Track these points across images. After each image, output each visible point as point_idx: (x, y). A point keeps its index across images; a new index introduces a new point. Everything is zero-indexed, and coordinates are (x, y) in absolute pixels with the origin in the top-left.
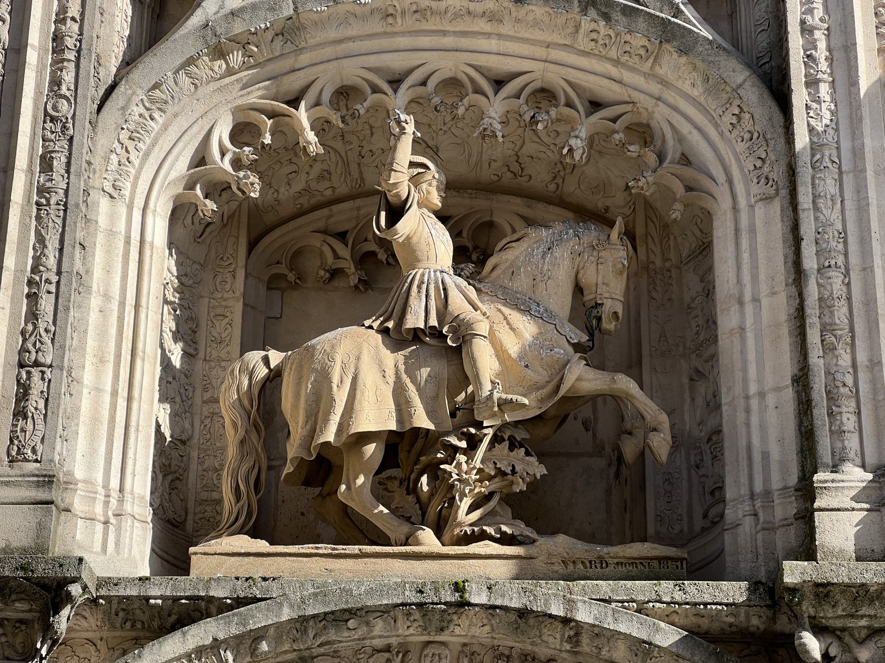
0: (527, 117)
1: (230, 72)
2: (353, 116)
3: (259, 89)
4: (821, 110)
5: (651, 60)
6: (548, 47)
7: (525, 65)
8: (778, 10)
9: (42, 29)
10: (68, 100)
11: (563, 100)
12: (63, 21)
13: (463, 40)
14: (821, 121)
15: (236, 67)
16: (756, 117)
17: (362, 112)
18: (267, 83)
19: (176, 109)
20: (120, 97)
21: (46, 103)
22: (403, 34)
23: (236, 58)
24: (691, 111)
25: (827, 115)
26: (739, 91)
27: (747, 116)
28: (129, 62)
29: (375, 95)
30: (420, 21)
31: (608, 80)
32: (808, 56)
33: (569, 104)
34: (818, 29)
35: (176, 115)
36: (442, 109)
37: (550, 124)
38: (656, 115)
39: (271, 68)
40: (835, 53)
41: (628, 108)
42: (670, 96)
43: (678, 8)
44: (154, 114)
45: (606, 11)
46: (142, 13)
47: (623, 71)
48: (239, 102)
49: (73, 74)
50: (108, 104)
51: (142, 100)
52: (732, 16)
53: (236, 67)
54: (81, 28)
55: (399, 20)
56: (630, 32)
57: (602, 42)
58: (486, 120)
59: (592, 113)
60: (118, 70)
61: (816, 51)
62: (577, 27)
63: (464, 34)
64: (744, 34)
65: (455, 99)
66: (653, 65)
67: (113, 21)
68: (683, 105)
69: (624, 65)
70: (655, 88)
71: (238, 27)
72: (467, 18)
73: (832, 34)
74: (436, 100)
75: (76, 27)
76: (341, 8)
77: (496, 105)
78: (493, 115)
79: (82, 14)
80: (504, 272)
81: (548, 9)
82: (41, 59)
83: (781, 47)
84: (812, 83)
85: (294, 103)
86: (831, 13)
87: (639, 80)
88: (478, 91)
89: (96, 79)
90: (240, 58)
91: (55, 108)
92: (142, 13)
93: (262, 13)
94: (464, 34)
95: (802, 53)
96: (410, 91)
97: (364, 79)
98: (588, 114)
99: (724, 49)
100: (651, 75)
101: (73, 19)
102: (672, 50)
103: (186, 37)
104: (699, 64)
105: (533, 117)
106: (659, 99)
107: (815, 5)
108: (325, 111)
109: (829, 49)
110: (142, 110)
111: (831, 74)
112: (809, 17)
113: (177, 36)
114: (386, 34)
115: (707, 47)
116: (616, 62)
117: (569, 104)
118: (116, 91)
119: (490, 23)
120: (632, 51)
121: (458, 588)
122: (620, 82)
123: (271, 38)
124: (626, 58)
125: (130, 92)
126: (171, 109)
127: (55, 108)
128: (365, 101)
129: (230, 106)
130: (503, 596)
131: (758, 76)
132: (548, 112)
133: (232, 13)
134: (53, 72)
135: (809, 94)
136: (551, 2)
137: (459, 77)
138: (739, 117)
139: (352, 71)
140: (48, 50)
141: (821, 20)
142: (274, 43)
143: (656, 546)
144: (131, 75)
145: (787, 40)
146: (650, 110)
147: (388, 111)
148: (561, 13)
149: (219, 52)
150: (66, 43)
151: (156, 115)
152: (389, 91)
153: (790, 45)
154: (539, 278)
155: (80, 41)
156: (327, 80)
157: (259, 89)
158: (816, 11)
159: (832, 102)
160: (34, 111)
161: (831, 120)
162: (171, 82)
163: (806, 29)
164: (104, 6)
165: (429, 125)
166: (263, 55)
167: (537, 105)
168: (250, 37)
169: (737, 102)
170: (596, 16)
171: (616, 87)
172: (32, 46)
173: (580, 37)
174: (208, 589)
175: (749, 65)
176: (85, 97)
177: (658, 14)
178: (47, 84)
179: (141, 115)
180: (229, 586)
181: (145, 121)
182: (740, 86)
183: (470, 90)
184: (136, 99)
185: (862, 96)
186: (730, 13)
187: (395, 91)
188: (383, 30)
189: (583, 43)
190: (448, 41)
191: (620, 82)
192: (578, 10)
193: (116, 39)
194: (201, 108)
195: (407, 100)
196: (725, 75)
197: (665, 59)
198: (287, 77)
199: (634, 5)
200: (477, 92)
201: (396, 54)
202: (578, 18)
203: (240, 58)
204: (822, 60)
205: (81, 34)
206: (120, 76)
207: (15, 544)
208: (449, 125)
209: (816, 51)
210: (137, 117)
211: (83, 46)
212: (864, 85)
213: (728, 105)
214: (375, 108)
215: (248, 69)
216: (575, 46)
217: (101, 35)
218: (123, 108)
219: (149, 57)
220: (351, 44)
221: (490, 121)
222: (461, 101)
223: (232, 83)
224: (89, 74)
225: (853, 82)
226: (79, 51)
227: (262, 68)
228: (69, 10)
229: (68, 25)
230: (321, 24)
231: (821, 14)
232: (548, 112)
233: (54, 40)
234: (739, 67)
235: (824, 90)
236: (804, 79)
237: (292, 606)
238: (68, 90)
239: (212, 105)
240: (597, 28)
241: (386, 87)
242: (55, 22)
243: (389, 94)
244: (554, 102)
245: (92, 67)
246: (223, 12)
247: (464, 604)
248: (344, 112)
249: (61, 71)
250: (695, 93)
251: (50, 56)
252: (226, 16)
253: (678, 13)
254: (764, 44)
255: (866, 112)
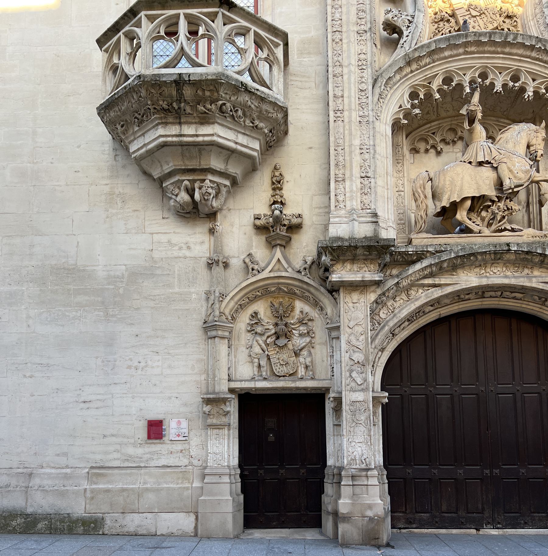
80: (503, 142)
121: (508, 245)
130: (522, 247)
143: (354, 279)
154: (516, 143)
174: (427, 248)
180: (434, 247)
207: (368, 236)
237: (454, 253)
247: (509, 250)
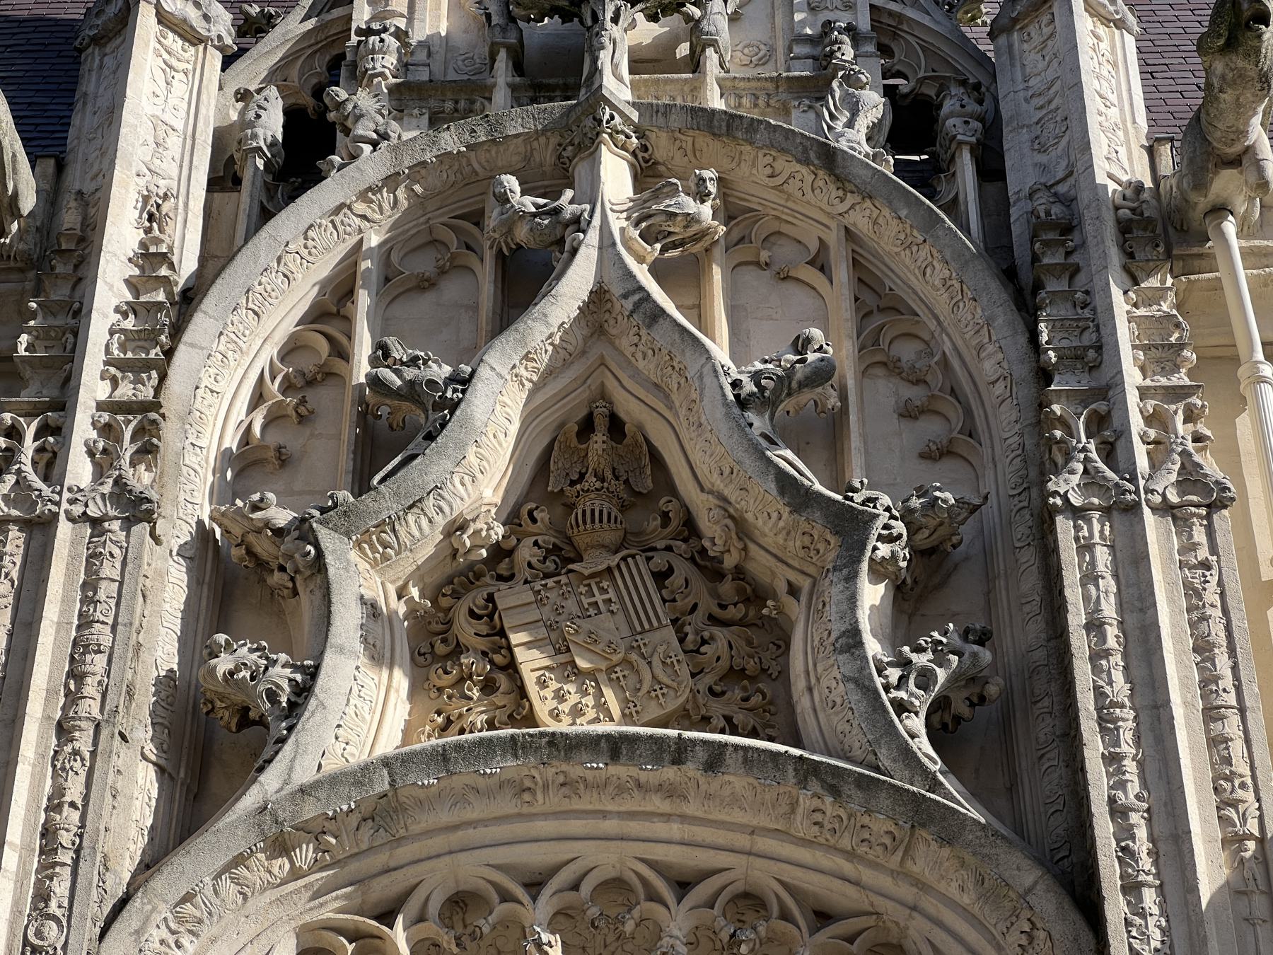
0: (725, 936)
1: (296, 874)
2: (473, 936)
3: (337, 898)
4: (1147, 928)
5: (900, 853)
6: (752, 833)
7: (722, 859)
8: (1076, 783)
9: (26, 819)
10: (58, 922)
11: (775, 910)
12: (58, 808)
13: (632, 824)
14: (1149, 944)
15: (305, 867)
16: (1056, 936)
17: (486, 929)
18: (349, 889)
19: (215, 930)
20: (134, 917)
21: (27, 927)
22: (545, 816)
23: (305, 854)
24: (962, 927)
25: (1157, 935)
26: (1028, 899)
27: (1041, 935)
28: (149, 865)
29: (505, 905)
30: (569, 797)
31: (840, 882)
32: (1124, 849)
33: (785, 916)
34: (1134, 810)
35: (213, 941)
36: (602, 924)
37: (758, 946)
38: (912, 932)
39: (354, 867)
40: (1160, 845)
41: (871, 921)
42: (929, 904)
43: (935, 779)
44: (181, 940)
45: (833, 782)
46: (173, 794)
47: (860, 868)
48: (307, 918)
49: (68, 884)
50: (116, 926)
51: (165, 919)
52: (1012, 789)
53: (305, 867)
54: (83, 818)
55: (540, 796)
56: (869, 812)
57: (830, 826)
58: (666, 941)
59: (819, 929)
60: (133, 876)
61: (1134, 842)
62: (794, 806)
63: (632, 815)
64: (1030, 816)
65: (620, 910)
66: (903, 859)
67: (130, 806)
68: (949, 917)
69: (862, 859)
70: (906, 891)
71: (310, 811)
72: (636, 793)
73: (1155, 817)
74: (594, 911)
75: (75, 816)
76: (457, 781)
77: (679, 918)
78: (676, 932)
79: (86, 798)
81: (751, 780)
82: (23, 864)
83: (1084, 835)
84: (1132, 888)
85: (387, 917)
86: (1151, 787)
87: (885, 882)
88: (654, 897)
89: (100, 890)
90: (310, 854)
91: (39, 934)
92: (173, 794)
93: (344, 790)
94: (632, 815)
95: (1114, 845)
96: (555, 898)
97: (489, 881)
98: (813, 932)
99: (1003, 837)
100: (900, 874)
101: (73, 805)
102: (930, 838)
103: (231, 825)
104: (969, 858)
105: (733, 935)
106: (914, 908)
107: (1127, 776)
108: (431, 929)
109: (1152, 838)
110: (164, 934)
111: (1157, 876)
112: (1120, 794)
113: (221, 824)
114: (520, 816)
115: (979, 834)
116: (850, 855)
117: (785, 916)
118: (128, 907)
119: (668, 800)
120: (872, 839)
122: (856, 883)
123: (355, 825)
124: (863, 849)
125: (149, 907)
126: (206, 931)
127: (39, 934)
128: (490, 914)
129: (293, 924)
131: (1054, 876)
132: (754, 928)
133: (302, 790)
134: (39, 882)
135: (1129, 903)
136: (755, 770)
137: (626, 878)
138: (1031, 938)
139: (471, 870)
140: (34, 850)
141: (1137, 797)
142: (360, 831)
144: (152, 884)
145: (1091, 826)
146: (902, 924)
147: (523, 929)
148: (770, 785)
149: (280, 847)
150: (60, 839)
151: (185, 940)
152: (525, 898)
153: (1097, 832)
155: (81, 836)
156: (437, 882)
157: (337, 898)
158: (1129, 784)
159: (1161, 915)
160: (8, 939)
161: (1163, 942)
162: (209, 891)
163: (1118, 811)
164: (119, 786)
165: (584, 948)
166: (344, 849)
167: (739, 916)
168: (326, 824)
169: (1026, 914)
170: (820, 791)
171: (851, 890)
172: (11, 844)
173: (799, 819)
175: (1039, 861)
176: (83, 917)
177: (907, 786)
178: (30, 900)
179: (162, 942)
181: (167, 950)
182: (1029, 890)
183: (642, 896)
184: (157, 918)
185: (1204, 906)
186: (1008, 785)
187: (534, 899)
188: (516, 810)
189: (801, 827)
190: (610, 826)
191: (856, 883)
192: (794, 781)
193: (133, 832)
194: (251, 929)
195: (551, 911)
196: (1006, 875)
197: (920, 850)
198: (378, 879)
199: (872, 774)
200: (652, 900)
201: (535, 846)
202: (794, 791)
203: (310, 854)
204: (1144, 855)
205: (83, 826)
206: (135, 886)
208: (611, 948)
209: (1134, 842)
210: (157, 945)
211: (85, 844)
212: (1206, 892)
213: (1014, 919)
214: (505, 923)
215: (322, 869)
216: (792, 831)
217: (112, 826)
218: (137, 932)
219: (179, 856)
220: (471, 831)
221: (672, 941)
222: (629, 911)
223: (298, 891)
224: (90, 884)
225: (1191, 887)
226: (78, 851)
227: (342, 868)
228: (68, 792)
229: (65, 814)
230: (426, 802)
231: (1137, 790)
232: (754, 928)
233: (43, 835)
234: (1026, 863)
235: (1149, 898)
236: (1119, 883)
238: (60, 907)
239: (267, 924)
240: (822, 807)
241: (520, 892)
242: (46, 810)
243: (526, 903)
244: (763, 912)
245: (96, 873)
246: (288, 789)
248: (460, 930)
249: (51, 880)
250: (966, 900)
251: (36, 859)
252: (293, 794)
253: (935, 786)
254: (1060, 831)
255: (1211, 929)
